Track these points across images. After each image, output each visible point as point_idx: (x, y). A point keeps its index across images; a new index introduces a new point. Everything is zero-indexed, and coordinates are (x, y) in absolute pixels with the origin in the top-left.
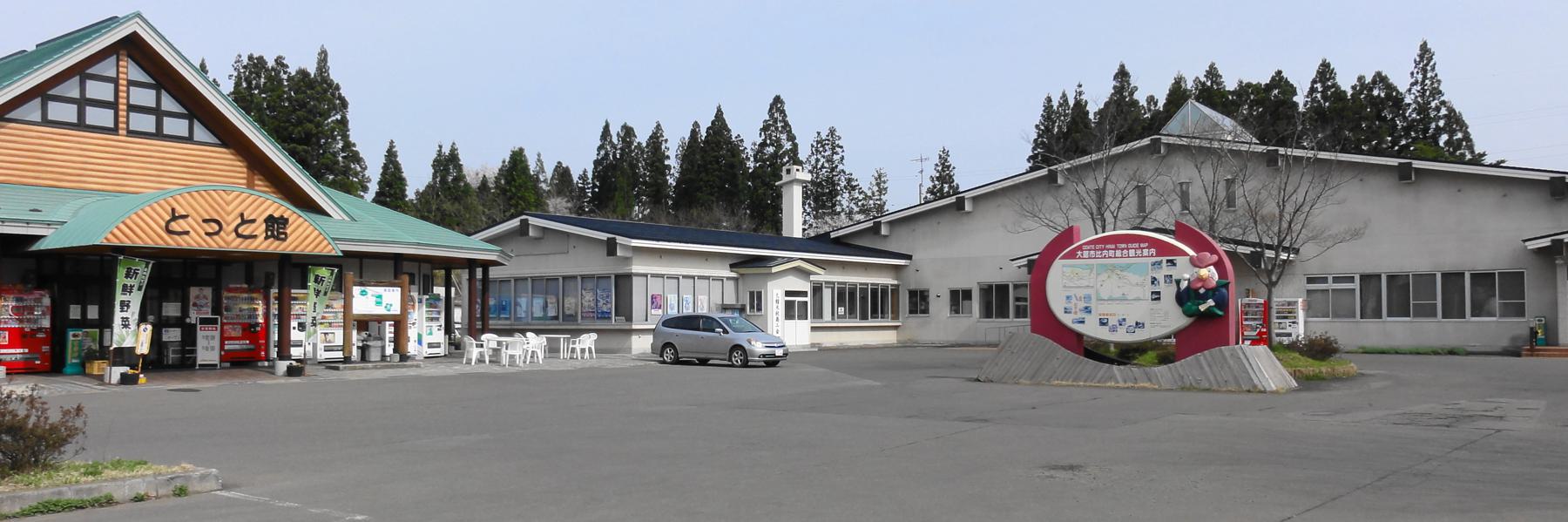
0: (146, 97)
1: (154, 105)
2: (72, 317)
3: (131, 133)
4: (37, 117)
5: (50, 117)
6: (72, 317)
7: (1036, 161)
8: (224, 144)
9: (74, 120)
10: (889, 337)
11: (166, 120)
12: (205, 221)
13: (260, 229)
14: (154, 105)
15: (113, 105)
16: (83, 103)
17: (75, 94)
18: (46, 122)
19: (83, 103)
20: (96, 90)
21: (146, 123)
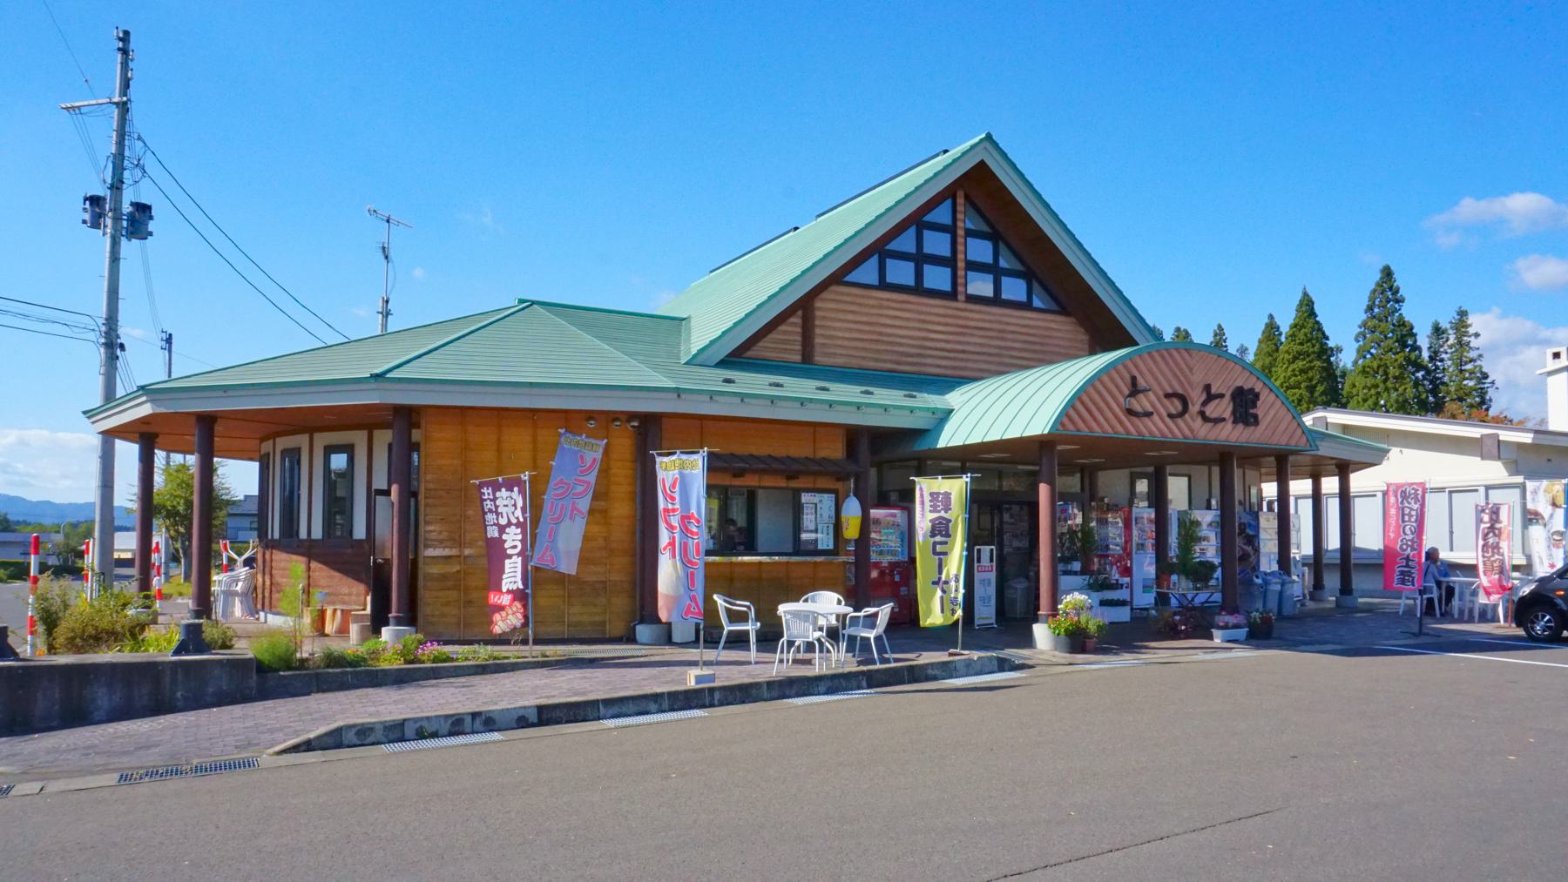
0: (981, 250)
1: (888, 261)
2: (1145, 481)
3: (972, 299)
4: (873, 279)
5: (890, 279)
6: (1145, 481)
7: (1402, 323)
8: (1063, 310)
9: (911, 282)
10: (61, 435)
11: (1005, 280)
12: (1167, 396)
13: (1223, 408)
14: (888, 261)
15: (950, 262)
16: (921, 259)
17: (912, 249)
18: (884, 285)
19: (921, 259)
20: (937, 244)
21: (981, 286)
